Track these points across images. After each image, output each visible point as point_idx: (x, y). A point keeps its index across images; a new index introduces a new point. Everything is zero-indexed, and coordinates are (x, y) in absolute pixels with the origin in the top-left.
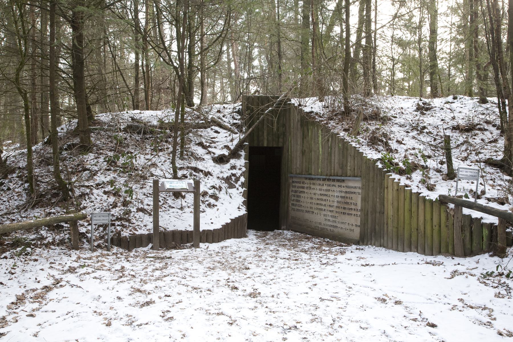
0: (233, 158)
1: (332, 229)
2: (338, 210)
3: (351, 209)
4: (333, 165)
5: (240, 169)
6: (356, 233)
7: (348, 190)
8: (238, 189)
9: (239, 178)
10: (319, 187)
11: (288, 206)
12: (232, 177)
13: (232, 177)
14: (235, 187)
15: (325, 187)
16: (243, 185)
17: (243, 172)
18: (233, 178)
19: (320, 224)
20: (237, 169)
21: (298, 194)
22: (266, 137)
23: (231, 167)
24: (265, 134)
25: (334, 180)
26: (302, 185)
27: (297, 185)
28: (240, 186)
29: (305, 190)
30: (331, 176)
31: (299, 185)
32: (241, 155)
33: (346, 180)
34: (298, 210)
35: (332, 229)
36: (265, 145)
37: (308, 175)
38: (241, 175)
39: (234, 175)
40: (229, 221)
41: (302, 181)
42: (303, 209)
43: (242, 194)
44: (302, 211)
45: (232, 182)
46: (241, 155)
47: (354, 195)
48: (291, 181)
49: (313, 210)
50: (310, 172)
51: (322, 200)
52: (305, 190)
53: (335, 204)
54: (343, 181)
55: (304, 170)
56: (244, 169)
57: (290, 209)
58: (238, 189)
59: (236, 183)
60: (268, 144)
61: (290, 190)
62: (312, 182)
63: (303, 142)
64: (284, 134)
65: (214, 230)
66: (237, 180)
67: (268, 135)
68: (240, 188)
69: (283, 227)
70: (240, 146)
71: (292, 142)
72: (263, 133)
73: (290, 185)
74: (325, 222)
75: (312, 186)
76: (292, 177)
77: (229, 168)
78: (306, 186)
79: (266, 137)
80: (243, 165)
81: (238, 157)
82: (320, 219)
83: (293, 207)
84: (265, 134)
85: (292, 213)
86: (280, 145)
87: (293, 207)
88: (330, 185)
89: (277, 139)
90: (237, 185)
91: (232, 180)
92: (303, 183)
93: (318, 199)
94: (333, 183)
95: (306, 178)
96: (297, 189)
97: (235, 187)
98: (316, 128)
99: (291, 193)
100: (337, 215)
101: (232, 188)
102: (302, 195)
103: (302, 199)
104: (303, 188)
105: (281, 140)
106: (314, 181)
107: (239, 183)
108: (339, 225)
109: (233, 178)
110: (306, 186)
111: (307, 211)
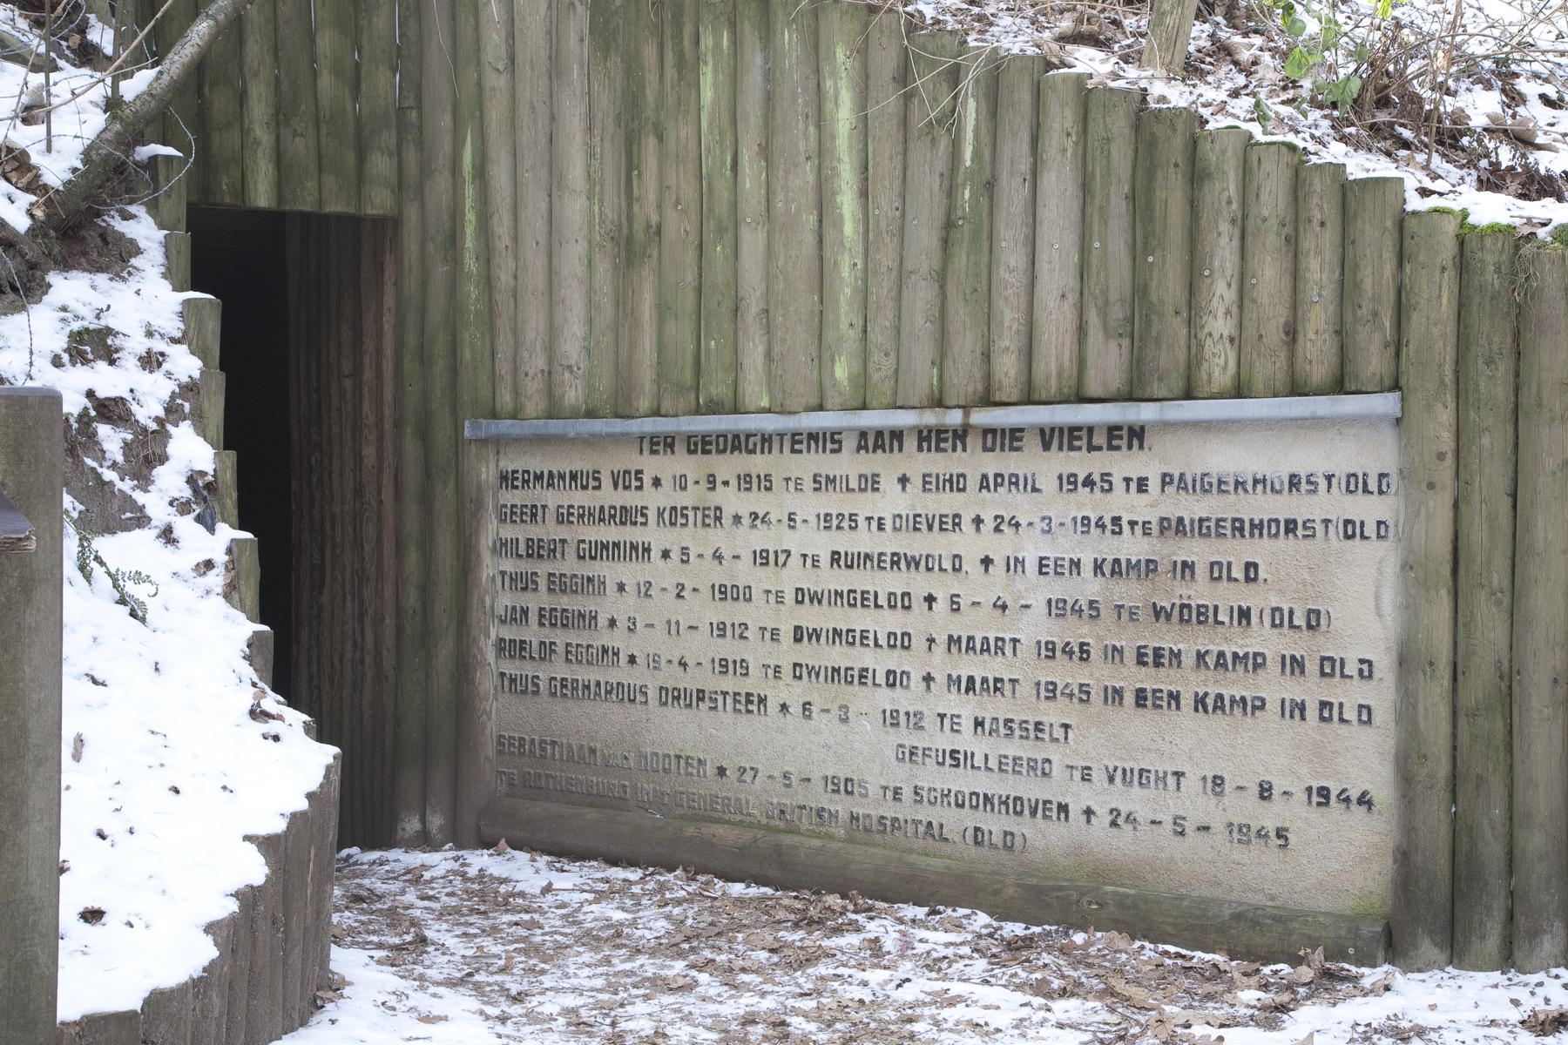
0: (66, 266)
1: (996, 824)
2: (1065, 673)
3: (1257, 662)
4: (1010, 317)
5: (151, 361)
6: (1343, 860)
7: (1193, 507)
8: (168, 535)
9: (162, 435)
10: (810, 505)
11: (464, 667)
12: (104, 430)
13: (104, 430)
14: (141, 520)
15: (891, 502)
16: (202, 497)
17: (189, 389)
18: (111, 439)
19: (846, 786)
20: (129, 362)
21: (568, 565)
22: (262, 134)
23: (78, 338)
24: (259, 109)
25: (1011, 438)
26: (610, 496)
27: (552, 498)
28: (183, 508)
29: (655, 536)
30: (987, 401)
31: (579, 498)
32: (133, 249)
33: (1167, 426)
34: (564, 689)
35: (996, 824)
36: (262, 196)
37: (698, 413)
38: (172, 411)
39: (111, 410)
40: (255, 869)
41: (608, 464)
42: (621, 674)
43: (216, 579)
44: (628, 695)
45: (109, 475)
46: (133, 249)
47: (1284, 544)
48: (487, 473)
49: (754, 684)
50: (717, 387)
51: (864, 600)
52: (655, 536)
53: (1034, 627)
54: (1137, 434)
55: (646, 375)
56: (186, 364)
57: (486, 683)
58: (168, 535)
59: (144, 482)
60: (280, 186)
61: (486, 540)
62: (727, 465)
63: (631, 164)
64: (407, 122)
65: (157, 1001)
66: (146, 454)
67: (281, 116)
68: (186, 527)
69: (412, 825)
70: (110, 176)
71: (500, 175)
72: (242, 96)
73: (479, 504)
74: (901, 775)
75: (732, 501)
76: (499, 443)
77: (60, 343)
78: (652, 499)
79: (262, 134)
80: (174, 327)
81: (115, 257)
82: (823, 750)
83: (511, 668)
84: (259, 109)
85: (499, 715)
86: (379, 202)
87: (511, 668)
88: (955, 483)
89: (350, 158)
90: (155, 503)
91: (101, 455)
92: (627, 479)
93: (800, 596)
94: (1009, 463)
95: (663, 443)
96: (561, 532)
97: (141, 520)
98: (789, 39)
99: (489, 566)
100: (1052, 714)
101: (111, 527)
102: (610, 571)
103: (607, 606)
104: (625, 516)
105: (381, 165)
106: (758, 463)
107: (170, 480)
108: (1080, 797)
109: (111, 439)
110: (652, 499)
111: (673, 696)
